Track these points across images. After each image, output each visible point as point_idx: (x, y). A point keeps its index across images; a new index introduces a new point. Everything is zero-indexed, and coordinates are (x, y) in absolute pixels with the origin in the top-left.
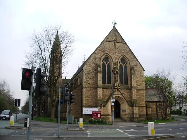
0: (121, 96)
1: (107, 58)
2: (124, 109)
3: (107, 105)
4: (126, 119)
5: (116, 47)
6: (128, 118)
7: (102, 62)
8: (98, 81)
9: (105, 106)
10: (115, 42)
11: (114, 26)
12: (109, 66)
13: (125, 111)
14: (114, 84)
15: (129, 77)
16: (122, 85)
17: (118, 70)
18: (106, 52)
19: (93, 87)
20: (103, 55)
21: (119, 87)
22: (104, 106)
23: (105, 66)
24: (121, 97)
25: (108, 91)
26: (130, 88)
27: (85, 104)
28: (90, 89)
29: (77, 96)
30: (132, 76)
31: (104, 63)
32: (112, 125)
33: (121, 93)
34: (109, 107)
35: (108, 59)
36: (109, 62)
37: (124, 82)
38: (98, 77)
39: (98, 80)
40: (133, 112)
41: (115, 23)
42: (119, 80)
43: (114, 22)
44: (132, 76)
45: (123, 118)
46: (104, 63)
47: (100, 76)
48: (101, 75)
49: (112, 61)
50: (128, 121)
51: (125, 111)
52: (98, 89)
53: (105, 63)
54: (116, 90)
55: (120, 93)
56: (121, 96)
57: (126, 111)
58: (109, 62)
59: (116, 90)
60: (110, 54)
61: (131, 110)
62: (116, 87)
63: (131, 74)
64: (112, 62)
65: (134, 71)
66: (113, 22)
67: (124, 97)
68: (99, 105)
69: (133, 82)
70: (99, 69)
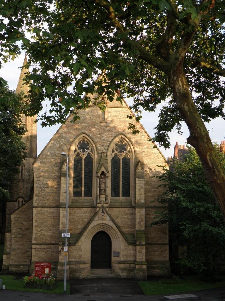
3: (79, 243)
6: (123, 270)
7: (113, 151)
8: (61, 194)
9: (75, 245)
12: (89, 160)
13: (118, 254)
17: (104, 170)
19: (54, 205)
21: (105, 205)
22: (74, 244)
24: (110, 226)
25: (85, 213)
28: (45, 209)
29: (26, 221)
32: (118, 258)
33: (110, 216)
34: (85, 246)
36: (88, 151)
40: (135, 256)
42: (109, 191)
44: (137, 179)
45: (114, 270)
46: (116, 155)
51: (118, 254)
53: (119, 154)
54: (99, 210)
55: (108, 218)
56: (111, 223)
57: (121, 255)
58: (88, 151)
59: (99, 210)
60: (91, 135)
61: (132, 252)
69: (137, 193)
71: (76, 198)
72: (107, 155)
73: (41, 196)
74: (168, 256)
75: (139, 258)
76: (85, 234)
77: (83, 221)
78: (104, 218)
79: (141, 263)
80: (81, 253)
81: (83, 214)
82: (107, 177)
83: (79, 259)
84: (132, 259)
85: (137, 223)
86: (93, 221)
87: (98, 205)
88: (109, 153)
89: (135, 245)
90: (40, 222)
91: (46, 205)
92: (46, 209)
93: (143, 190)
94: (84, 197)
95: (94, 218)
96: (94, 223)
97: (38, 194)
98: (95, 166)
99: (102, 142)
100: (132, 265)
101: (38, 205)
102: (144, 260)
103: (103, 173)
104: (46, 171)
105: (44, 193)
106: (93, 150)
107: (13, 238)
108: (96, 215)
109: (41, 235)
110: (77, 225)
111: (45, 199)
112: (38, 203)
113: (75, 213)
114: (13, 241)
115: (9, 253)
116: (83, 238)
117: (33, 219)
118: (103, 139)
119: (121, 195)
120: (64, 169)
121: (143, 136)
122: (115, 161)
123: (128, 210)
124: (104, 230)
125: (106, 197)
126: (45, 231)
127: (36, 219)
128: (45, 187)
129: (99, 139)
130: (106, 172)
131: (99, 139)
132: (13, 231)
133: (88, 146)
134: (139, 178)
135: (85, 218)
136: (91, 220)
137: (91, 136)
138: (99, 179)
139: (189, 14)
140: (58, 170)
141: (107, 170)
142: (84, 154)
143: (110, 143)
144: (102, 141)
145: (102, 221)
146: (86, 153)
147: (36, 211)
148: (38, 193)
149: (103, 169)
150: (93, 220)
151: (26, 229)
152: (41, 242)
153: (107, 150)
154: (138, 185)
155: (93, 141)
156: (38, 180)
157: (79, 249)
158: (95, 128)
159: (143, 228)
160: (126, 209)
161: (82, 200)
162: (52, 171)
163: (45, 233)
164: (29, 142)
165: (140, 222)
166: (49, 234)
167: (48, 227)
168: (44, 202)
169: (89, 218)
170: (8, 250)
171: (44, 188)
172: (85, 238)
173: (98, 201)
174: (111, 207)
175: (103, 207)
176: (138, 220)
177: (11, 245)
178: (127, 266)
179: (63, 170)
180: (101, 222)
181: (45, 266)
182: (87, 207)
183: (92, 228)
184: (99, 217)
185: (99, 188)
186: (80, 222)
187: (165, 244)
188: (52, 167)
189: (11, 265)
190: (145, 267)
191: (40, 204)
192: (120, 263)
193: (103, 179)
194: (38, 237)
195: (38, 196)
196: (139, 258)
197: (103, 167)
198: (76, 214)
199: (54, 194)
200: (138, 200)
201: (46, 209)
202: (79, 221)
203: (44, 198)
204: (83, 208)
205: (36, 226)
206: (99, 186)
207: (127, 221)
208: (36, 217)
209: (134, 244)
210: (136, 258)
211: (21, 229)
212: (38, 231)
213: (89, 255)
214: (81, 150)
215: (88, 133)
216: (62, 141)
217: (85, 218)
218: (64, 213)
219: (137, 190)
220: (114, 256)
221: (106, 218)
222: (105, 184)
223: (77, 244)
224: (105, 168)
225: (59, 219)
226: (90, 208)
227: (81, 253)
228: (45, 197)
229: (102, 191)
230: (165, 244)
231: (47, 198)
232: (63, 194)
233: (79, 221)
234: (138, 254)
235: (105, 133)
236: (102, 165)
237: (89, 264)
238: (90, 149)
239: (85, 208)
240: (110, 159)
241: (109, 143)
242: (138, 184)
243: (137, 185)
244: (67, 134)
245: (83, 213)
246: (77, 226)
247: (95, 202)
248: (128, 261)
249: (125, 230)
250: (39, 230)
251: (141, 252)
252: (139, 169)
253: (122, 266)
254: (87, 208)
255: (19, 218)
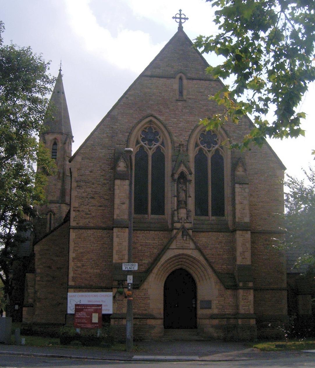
0: (196, 254)
1: (150, 134)
2: (206, 299)
3: (145, 286)
4: (211, 330)
5: (185, 92)
6: (216, 327)
7: (197, 145)
8: (116, 206)
10: (181, 79)
11: (180, 28)
12: (159, 157)
13: (208, 304)
14: (173, 215)
15: (227, 191)
16: (203, 218)
17: (185, 169)
18: (149, 112)
20: (139, 123)
21: (188, 226)
23: (147, 156)
24: (194, 258)
26: (231, 229)
27: (74, 279)
28: (90, 232)
30: (237, 186)
31: (142, 147)
32: (210, 310)
33: (195, 243)
34: (154, 290)
35: (157, 133)
36: (158, 144)
37: (210, 208)
38: (117, 192)
39: (117, 201)
40: (237, 307)
41: (183, 16)
42: (191, 203)
43: (180, 15)
44: (237, 186)
47: (123, 190)
48: (127, 187)
49: (169, 141)
50: (219, 338)
52: (115, 230)
53: (147, 147)
54: (177, 233)
55: (192, 245)
56: (196, 254)
57: (214, 306)
58: (158, 144)
62: (178, 225)
63: (234, 181)
64: (170, 144)
65: (245, 170)
66: (178, 16)
67: (206, 259)
68: (116, 283)
69: (238, 207)
70: (122, 166)
71: (139, 216)
72: (187, 150)
73: (83, 211)
74: (286, 307)
75: (244, 308)
76: (155, 270)
77: (150, 252)
78: (186, 245)
79: (247, 317)
80: (149, 301)
81: (150, 242)
82: (190, 181)
83: (146, 310)
84: (231, 310)
85: (238, 254)
86: (168, 250)
87: (175, 225)
88: (192, 146)
89: (235, 289)
90: (81, 253)
91: (92, 225)
92: (92, 232)
93: (246, 202)
94: (152, 215)
95: (169, 246)
96: (169, 254)
97: (77, 208)
98: (168, 166)
99: (180, 129)
100: (232, 321)
101: (77, 225)
102: (252, 311)
103: (182, 176)
104: (91, 172)
105: (87, 207)
106: (165, 141)
107: (38, 281)
108: (172, 242)
109: (82, 272)
110: (141, 258)
111: (89, 216)
112: (77, 222)
113: (137, 240)
114: (37, 287)
115: (31, 306)
116: (152, 278)
117: (70, 247)
118: (180, 125)
119: (210, 213)
120: (119, 167)
121: (243, 123)
122: (200, 159)
123: (222, 236)
124: (184, 267)
125: (188, 212)
126: (89, 267)
127: (75, 247)
128: (89, 197)
129: (175, 125)
130: (188, 173)
131: (175, 125)
132: (38, 271)
133: (158, 137)
134: (240, 184)
135: (153, 247)
136: (165, 249)
137: (162, 119)
138: (176, 185)
139: (256, 81)
140: (109, 171)
141: (188, 168)
142: (150, 149)
143: (192, 132)
144: (179, 128)
145: (181, 248)
146: (154, 147)
147: (74, 234)
148: (77, 205)
149: (183, 168)
150: (168, 249)
151: (58, 268)
152: (83, 285)
153: (188, 141)
154: (239, 195)
155: (165, 127)
156: (78, 186)
157: (145, 294)
158: (169, 108)
159: (249, 262)
160: (219, 234)
161: (148, 220)
162: (100, 172)
163: (89, 270)
164: (60, 181)
165: (244, 252)
166: (95, 271)
167: (94, 260)
168: (87, 220)
169: (159, 247)
170: (31, 301)
171: (87, 199)
172: (155, 278)
173: (176, 219)
174: (196, 230)
175: (183, 228)
176: (239, 250)
177: (35, 292)
178: (224, 322)
179: (119, 169)
180: (181, 253)
181: (92, 309)
182: (156, 231)
183: (166, 261)
184: (177, 243)
185: (176, 198)
186: (145, 254)
187: (281, 289)
188: (100, 166)
189: (35, 324)
190: (253, 322)
191: (81, 224)
192: (212, 317)
193: (183, 185)
194: (78, 276)
195: (78, 211)
196: (244, 308)
197: (182, 165)
198: (140, 241)
199: (104, 208)
200: (239, 218)
201: (92, 232)
202: (145, 253)
203: (87, 214)
204: (151, 232)
205: (74, 259)
206: (176, 194)
207: (221, 253)
208: (75, 244)
209: (235, 287)
210: (238, 309)
211: (50, 267)
212: (78, 267)
213: (161, 306)
214: (146, 142)
215: (157, 115)
216: (116, 127)
217: (153, 247)
218: (121, 239)
219: (237, 202)
220: (201, 308)
221: (188, 245)
222: (185, 191)
223: (141, 288)
224: (186, 167)
225: (111, 248)
226: (161, 232)
227: (149, 301)
228: (89, 213)
229: (182, 204)
230: (281, 289)
231: (93, 214)
232: (119, 205)
233: (145, 253)
234: (242, 303)
235: (185, 116)
236: (181, 161)
237: (161, 320)
238: (161, 140)
239: (153, 232)
240: (192, 154)
241: (191, 131)
242: (239, 192)
243: (237, 194)
244: (125, 117)
245: (150, 240)
246: (142, 260)
247: (169, 221)
248: (225, 314)
249: (217, 267)
250: (79, 264)
251: (245, 298)
252: (240, 172)
253: (216, 322)
254: (156, 232)
255: (47, 250)
